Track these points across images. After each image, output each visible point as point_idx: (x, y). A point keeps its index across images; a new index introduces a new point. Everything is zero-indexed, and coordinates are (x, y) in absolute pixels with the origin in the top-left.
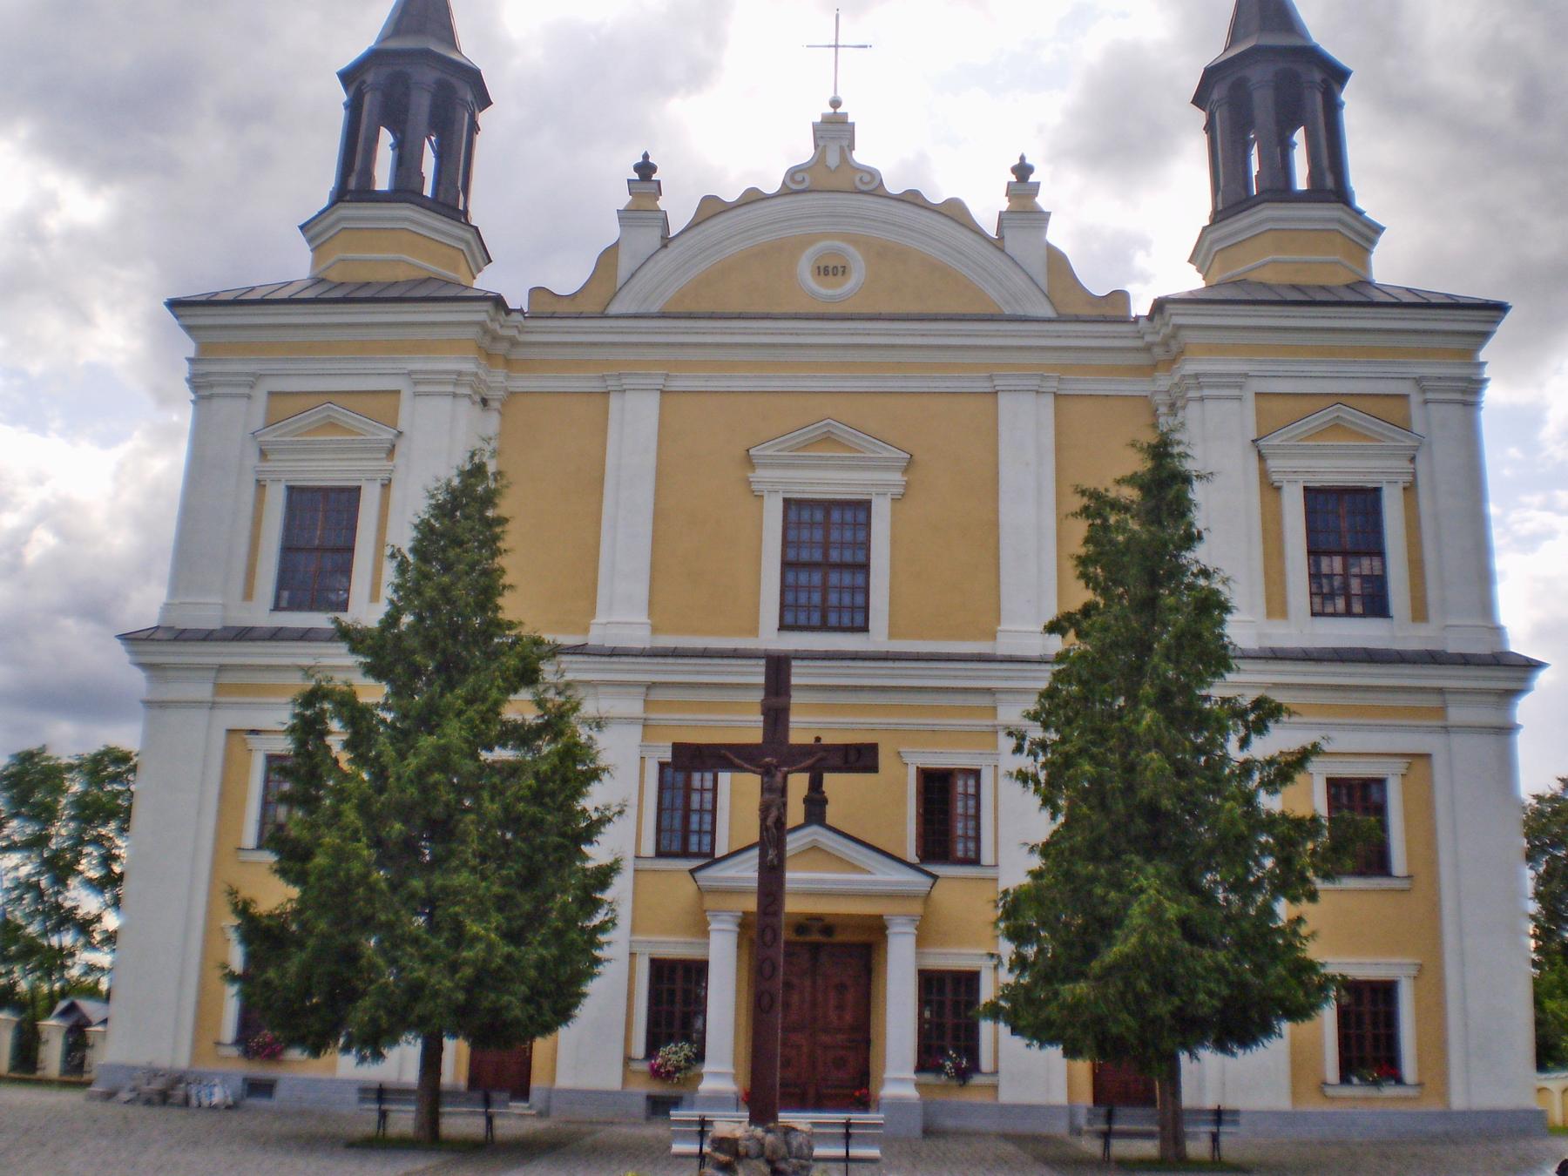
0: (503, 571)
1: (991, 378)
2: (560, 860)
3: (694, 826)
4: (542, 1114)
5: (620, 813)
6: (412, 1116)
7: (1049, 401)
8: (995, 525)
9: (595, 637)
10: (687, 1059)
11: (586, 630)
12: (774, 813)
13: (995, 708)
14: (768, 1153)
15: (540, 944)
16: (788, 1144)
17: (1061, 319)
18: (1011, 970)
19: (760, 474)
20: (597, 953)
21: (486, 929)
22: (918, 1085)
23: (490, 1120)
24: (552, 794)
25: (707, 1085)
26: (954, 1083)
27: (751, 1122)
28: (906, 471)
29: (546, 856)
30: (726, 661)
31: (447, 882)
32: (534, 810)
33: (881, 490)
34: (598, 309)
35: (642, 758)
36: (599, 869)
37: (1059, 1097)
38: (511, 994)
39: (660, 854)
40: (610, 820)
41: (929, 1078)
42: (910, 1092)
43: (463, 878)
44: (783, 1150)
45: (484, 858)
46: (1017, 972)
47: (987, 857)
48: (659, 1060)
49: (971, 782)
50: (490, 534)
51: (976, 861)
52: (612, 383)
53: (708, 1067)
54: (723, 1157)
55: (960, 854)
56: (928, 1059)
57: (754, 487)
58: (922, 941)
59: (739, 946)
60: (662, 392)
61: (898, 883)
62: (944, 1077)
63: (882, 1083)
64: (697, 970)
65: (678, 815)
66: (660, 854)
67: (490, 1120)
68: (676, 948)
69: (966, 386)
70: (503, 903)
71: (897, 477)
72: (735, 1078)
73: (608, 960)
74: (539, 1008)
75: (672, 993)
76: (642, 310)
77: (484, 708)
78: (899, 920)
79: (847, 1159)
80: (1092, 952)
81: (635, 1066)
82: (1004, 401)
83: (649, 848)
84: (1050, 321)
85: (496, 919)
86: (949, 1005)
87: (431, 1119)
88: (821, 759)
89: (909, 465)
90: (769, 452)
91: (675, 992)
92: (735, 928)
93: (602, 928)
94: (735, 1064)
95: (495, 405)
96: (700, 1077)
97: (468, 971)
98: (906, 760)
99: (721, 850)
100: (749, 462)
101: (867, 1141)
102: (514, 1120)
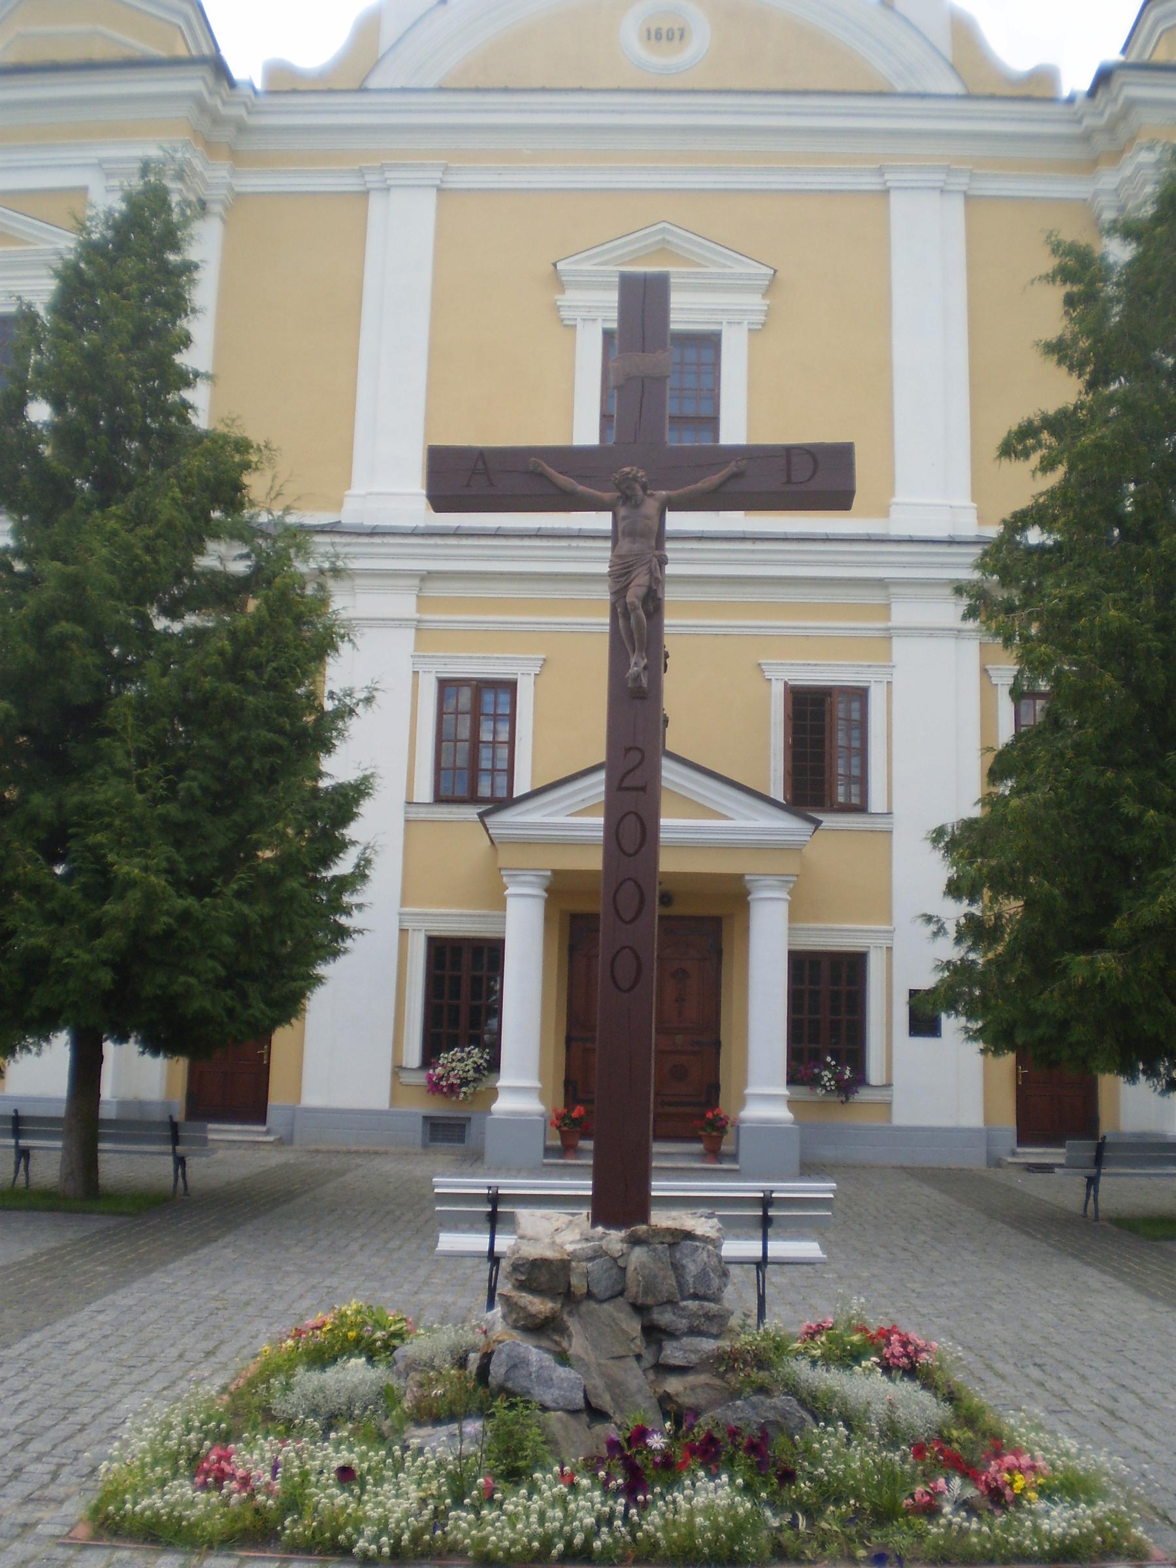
0: (713, 1476)
1: (880, 171)
2: (273, 770)
3: (485, 764)
4: (282, 1142)
5: (368, 700)
6: (58, 1156)
7: (957, 206)
8: (885, 367)
9: (349, 515)
10: (477, 1069)
11: (339, 505)
12: (640, 581)
13: (888, 607)
14: (633, 1289)
15: (240, 895)
16: (677, 1268)
17: (969, 97)
18: (958, 940)
19: (571, 298)
20: (343, 920)
21: (146, 869)
22: (792, 1104)
23: (180, 1162)
24: (258, 667)
25: (503, 1105)
26: (834, 1098)
27: (595, 1222)
28: (768, 291)
29: (249, 760)
30: (527, 542)
31: (88, 798)
32: (231, 688)
33: (736, 318)
34: (356, 86)
35: (416, 673)
36: (340, 789)
37: (972, 1117)
38: (192, 973)
39: (440, 799)
40: (352, 712)
41: (802, 1092)
42: (781, 1113)
43: (108, 792)
44: (669, 1283)
45: (142, 758)
46: (969, 942)
47: (877, 802)
48: (439, 1070)
49: (856, 705)
50: (167, 290)
51: (862, 808)
52: (373, 179)
53: (505, 1079)
54: (540, 1306)
55: (841, 799)
56: (801, 1069)
57: (564, 314)
58: (799, 910)
59: (547, 919)
60: (440, 190)
61: (764, 831)
62: (820, 1091)
63: (742, 1101)
64: (489, 953)
65: (464, 747)
66: (440, 799)
67: (180, 1162)
68: (460, 921)
69: (847, 182)
70: (179, 833)
71: (756, 301)
72: (542, 1098)
73: (360, 932)
74: (243, 996)
75: (456, 981)
76: (413, 84)
77: (151, 532)
78: (770, 881)
79: (762, 1263)
80: (1109, 912)
81: (406, 1078)
82: (897, 202)
83: (424, 790)
84: (957, 97)
85: (163, 851)
86: (828, 996)
87: (85, 1160)
88: (735, 476)
89: (771, 287)
90: (586, 267)
91: (461, 982)
92: (540, 892)
93: (345, 884)
94: (542, 1077)
95: (216, 208)
96: (493, 1094)
97: (116, 937)
98: (768, 675)
99: (522, 786)
100: (558, 282)
101: (798, 1229)
102: (230, 1152)
